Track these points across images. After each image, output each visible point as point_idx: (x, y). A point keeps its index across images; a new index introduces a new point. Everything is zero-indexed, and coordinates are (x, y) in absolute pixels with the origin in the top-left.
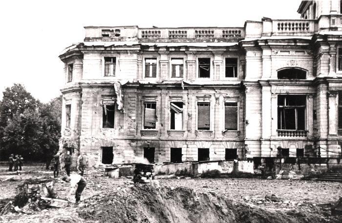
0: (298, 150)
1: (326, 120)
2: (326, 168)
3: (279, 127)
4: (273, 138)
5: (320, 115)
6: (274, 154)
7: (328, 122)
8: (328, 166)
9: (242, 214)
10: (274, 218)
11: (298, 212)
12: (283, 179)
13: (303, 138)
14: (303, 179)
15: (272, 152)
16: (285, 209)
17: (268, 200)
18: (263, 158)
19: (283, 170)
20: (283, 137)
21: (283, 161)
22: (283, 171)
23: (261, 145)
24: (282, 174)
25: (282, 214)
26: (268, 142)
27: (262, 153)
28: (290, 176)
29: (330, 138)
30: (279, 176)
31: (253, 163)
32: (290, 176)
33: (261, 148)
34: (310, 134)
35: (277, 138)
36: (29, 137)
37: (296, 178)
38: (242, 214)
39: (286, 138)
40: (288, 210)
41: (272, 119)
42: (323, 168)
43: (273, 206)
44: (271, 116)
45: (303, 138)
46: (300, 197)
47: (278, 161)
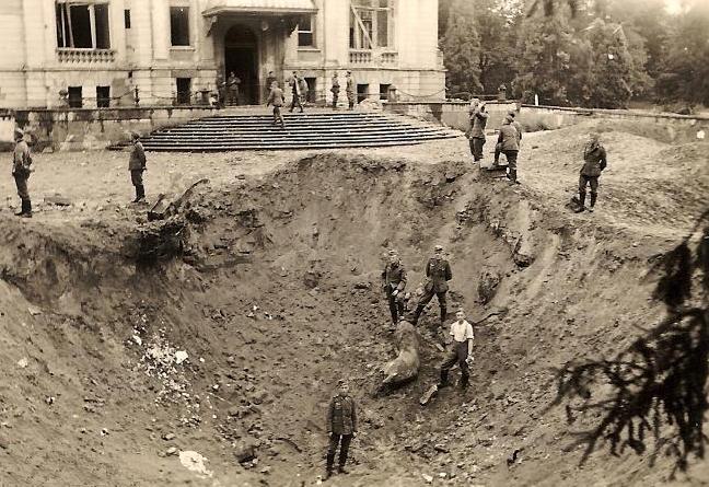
0: (99, 89)
1: (149, 30)
2: (150, 126)
3: (60, 44)
4: (49, 66)
5: (137, 35)
6: (52, 101)
7: (152, 26)
8: (152, 123)
9: (9, 235)
10: (61, 234)
11: (98, 221)
12: (72, 150)
13: (109, 65)
14: (110, 149)
15: (49, 95)
16: (77, 217)
17: (50, 205)
18: (33, 110)
19: (72, 133)
20: (69, 65)
21: (71, 116)
22: (72, 137)
23: (25, 80)
24: (72, 141)
25: (73, 228)
26: (40, 74)
27: (30, 97)
28: (86, 144)
29: (157, 65)
30: (65, 146)
31: (13, 120)
32: (86, 144)
33: (25, 87)
34: (120, 57)
35: (57, 65)
36: (573, 390)
37: (97, 147)
38: (9, 235)
39: (75, 65)
40: (83, 219)
41: (46, 27)
42: (145, 127)
43: (58, 215)
44: (43, 21)
45: (109, 65)
46: (102, 189)
47: (62, 117)
